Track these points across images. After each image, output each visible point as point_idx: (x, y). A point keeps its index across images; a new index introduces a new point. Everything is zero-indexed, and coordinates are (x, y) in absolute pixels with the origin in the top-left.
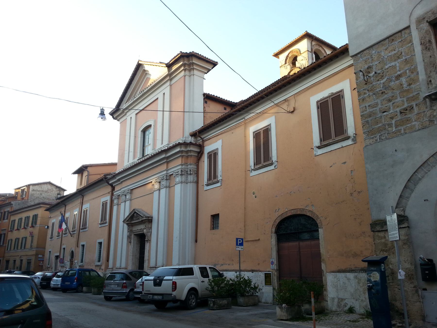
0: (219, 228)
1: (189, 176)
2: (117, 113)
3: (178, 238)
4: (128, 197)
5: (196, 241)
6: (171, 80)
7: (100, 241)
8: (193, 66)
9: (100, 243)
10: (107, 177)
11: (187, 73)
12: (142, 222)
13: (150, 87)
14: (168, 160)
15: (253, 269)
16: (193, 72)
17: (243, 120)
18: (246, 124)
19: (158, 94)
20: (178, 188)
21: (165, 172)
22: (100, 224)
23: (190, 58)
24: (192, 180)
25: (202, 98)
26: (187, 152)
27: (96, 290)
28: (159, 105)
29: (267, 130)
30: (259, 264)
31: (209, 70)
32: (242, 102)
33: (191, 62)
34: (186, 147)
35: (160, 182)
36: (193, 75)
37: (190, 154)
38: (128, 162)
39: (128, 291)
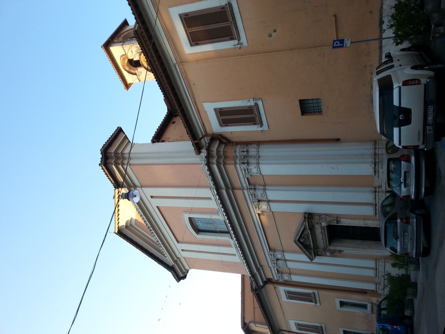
1: (250, 154)
2: (180, 275)
4: (279, 256)
5: (338, 140)
8: (119, 154)
9: (342, 304)
10: (254, 288)
11: (126, 162)
12: (312, 228)
13: (144, 217)
15: (378, 23)
16: (126, 154)
17: (177, 66)
18: (182, 61)
19: (152, 205)
20: (268, 170)
22: (316, 303)
23: (108, 155)
25: (157, 144)
26: (219, 157)
27: (410, 290)
28: (166, 205)
29: (188, 20)
30: (371, 12)
32: (167, 100)
33: (113, 155)
34: (213, 157)
35: (259, 201)
37: (222, 153)
38: (235, 255)
39: (414, 215)
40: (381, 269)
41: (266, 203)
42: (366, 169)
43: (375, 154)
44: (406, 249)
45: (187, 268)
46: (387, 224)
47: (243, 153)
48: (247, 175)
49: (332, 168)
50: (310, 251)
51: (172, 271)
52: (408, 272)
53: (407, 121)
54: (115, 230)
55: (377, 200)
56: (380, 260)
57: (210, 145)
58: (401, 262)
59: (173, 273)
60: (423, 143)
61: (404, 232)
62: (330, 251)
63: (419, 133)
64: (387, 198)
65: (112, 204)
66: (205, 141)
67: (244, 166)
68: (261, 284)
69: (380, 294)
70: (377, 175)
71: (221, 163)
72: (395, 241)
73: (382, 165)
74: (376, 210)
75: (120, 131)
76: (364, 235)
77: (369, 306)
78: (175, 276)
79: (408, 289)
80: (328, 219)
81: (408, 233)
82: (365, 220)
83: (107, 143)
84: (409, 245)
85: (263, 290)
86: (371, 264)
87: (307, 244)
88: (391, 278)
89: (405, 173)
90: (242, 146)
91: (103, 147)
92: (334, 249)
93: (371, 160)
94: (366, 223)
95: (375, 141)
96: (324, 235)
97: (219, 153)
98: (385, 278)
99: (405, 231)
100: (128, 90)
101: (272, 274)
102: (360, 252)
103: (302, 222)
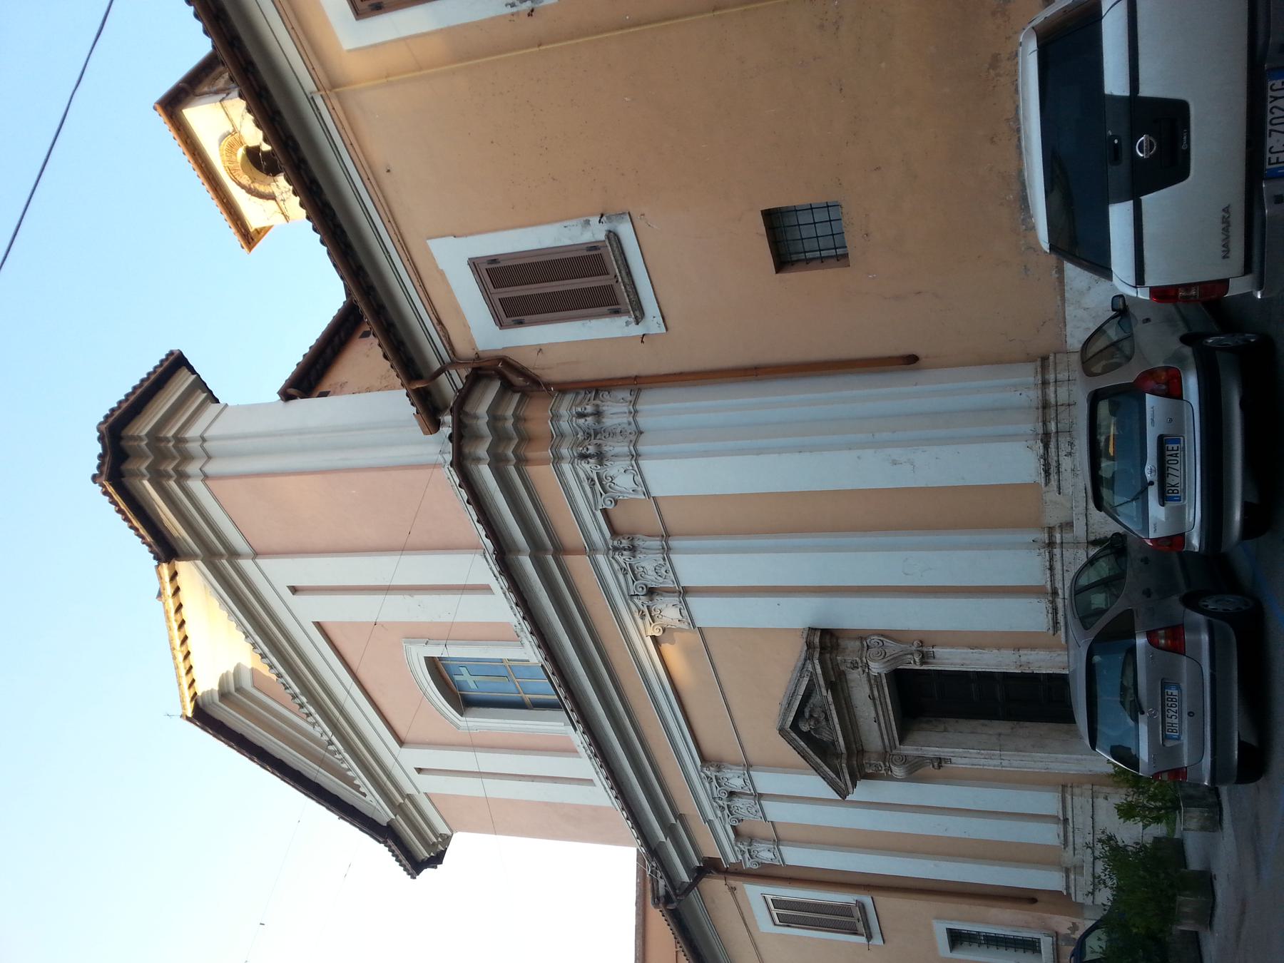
0: (831, 199)
1: (608, 422)
2: (417, 851)
3: (896, 453)
4: (737, 783)
5: (911, 360)
6: (233, 554)
7: (943, 941)
8: (167, 440)
9: (956, 938)
10: (662, 892)
11: (193, 468)
12: (837, 683)
14: (548, 547)
16: (194, 440)
17: (319, 102)
18: (332, 85)
19: (300, 617)
21: (601, 558)
22: (869, 937)
23: (126, 444)
24: (624, 408)
25: (300, 404)
26: (500, 437)
27: (1187, 902)
31: (200, 385)
33: (143, 444)
34: (478, 437)
35: (651, 592)
36: (204, 440)
37: (509, 424)
39: (1200, 618)
40: (1081, 819)
41: (676, 600)
42: (1015, 463)
43: (1045, 406)
44: (1175, 752)
45: (443, 829)
46: (1097, 659)
47: (581, 421)
48: (600, 500)
49: (894, 463)
50: (837, 762)
51: (390, 842)
52: (1174, 831)
53: (1170, 165)
54: (184, 708)
55: (1058, 577)
56: (1076, 791)
57: (464, 396)
58: (1152, 798)
59: (394, 847)
60: (1247, 269)
61: (1165, 685)
62: (905, 760)
63: (1226, 222)
64: (1091, 562)
65: (157, 613)
66: (450, 385)
67: (587, 467)
68: (685, 877)
69: (1082, 905)
70: (1054, 483)
71: (507, 460)
72: (1131, 723)
73: (1071, 444)
74: (1055, 611)
75: (176, 363)
76: (1022, 701)
77: (1046, 944)
78: (402, 857)
79: (1180, 899)
80: (892, 648)
81: (1178, 688)
82: (1018, 648)
83: (124, 406)
84: (1185, 739)
85: (693, 895)
86: (1048, 802)
87: (823, 738)
88: (1115, 853)
89: (1162, 441)
90: (580, 397)
91: (107, 417)
92: (919, 753)
93: (1030, 425)
94: (1024, 659)
95: (1044, 359)
96: (884, 705)
97: (500, 424)
98: (1097, 854)
99: (1165, 683)
100: (250, 249)
101: (715, 840)
102: (1005, 763)
103: (800, 664)
